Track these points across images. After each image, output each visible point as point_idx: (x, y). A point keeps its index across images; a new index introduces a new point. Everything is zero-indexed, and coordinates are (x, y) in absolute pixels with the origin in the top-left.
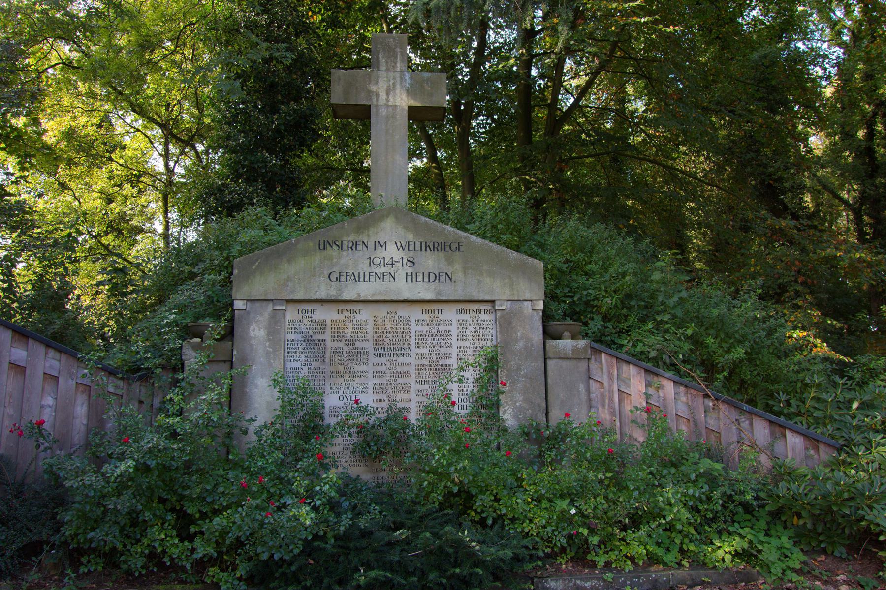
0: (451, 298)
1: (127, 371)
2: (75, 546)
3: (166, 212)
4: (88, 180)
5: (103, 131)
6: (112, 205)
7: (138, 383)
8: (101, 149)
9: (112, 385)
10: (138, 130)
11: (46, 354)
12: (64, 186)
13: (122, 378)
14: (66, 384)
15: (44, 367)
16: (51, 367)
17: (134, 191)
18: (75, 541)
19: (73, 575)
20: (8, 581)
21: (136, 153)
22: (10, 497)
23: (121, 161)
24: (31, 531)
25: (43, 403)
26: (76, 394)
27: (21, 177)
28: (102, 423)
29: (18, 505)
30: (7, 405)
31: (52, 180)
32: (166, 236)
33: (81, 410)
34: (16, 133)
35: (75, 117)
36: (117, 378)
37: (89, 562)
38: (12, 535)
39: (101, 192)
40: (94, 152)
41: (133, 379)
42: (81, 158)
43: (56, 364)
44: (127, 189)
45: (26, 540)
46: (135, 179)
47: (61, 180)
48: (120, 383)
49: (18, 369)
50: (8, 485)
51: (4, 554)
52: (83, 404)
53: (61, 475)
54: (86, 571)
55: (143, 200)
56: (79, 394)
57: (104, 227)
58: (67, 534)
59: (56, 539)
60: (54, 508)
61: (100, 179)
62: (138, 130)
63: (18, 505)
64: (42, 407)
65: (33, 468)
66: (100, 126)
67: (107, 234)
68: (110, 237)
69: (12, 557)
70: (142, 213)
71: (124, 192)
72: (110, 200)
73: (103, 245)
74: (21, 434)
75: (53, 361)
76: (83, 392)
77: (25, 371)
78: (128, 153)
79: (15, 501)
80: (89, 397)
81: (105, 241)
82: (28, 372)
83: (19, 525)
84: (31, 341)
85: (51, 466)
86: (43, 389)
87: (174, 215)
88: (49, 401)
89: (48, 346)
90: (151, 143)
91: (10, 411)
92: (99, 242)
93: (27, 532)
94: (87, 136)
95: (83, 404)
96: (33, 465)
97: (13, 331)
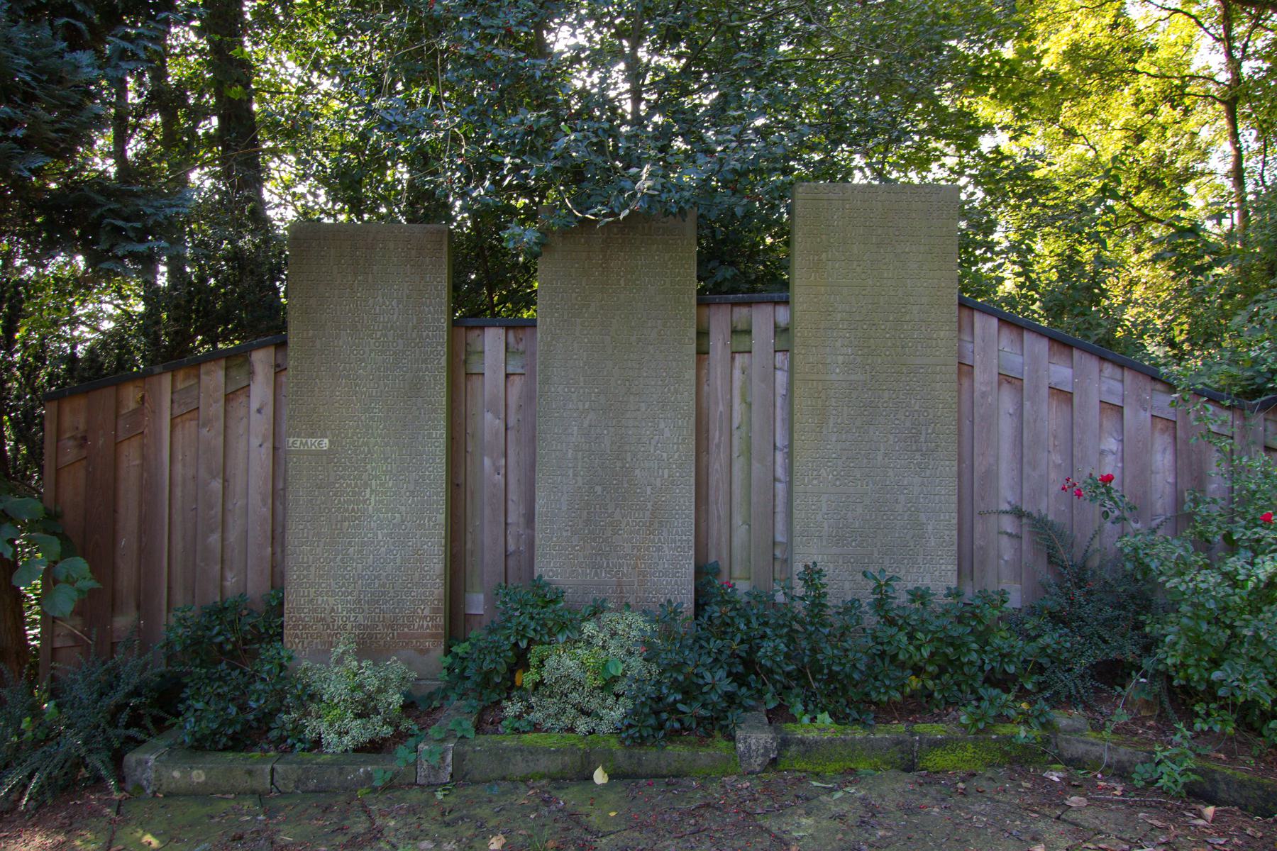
0: (174, 511)
1: (1237, 395)
2: (1183, 682)
3: (1235, 135)
4: (1103, 115)
5: (1120, 32)
6: (1143, 145)
7: (1262, 415)
8: (1121, 60)
9: (1217, 419)
10: (1176, 11)
11: (1101, 371)
12: (1070, 133)
13: (1228, 408)
14: (1136, 418)
15: (1100, 392)
16: (1110, 392)
17: (1178, 113)
18: (1181, 674)
19: (1188, 734)
20: (1080, 710)
21: (1175, 50)
22: (1069, 584)
23: (1153, 71)
24: (1105, 641)
25: (1102, 447)
26: (1153, 433)
27: (1021, 128)
28: (1200, 481)
29: (1082, 599)
30: (1051, 449)
31: (1055, 128)
32: (1238, 174)
33: (1162, 460)
34: (1007, 68)
35: (1078, 25)
36: (1222, 407)
37: (1208, 714)
38: (1078, 643)
39: (1125, 128)
40: (1111, 68)
41: (1252, 409)
42: (1093, 83)
43: (1117, 386)
44: (1166, 113)
45: (1100, 656)
46: (1175, 96)
47: (1067, 126)
48: (1226, 416)
49: (1062, 395)
50: (1065, 568)
51: (1070, 670)
52: (1165, 449)
53: (1153, 566)
54: (1206, 728)
55: (1191, 125)
56: (1157, 434)
57: (1134, 182)
58: (1169, 661)
59: (1147, 663)
60: (1138, 613)
61: (1122, 109)
62: (1176, 11)
63: (1082, 599)
64: (1102, 453)
65: (1096, 545)
66: (1114, 26)
67: (1139, 190)
68: (1144, 195)
69: (1082, 677)
70: (1190, 147)
71: (1161, 120)
72: (1139, 137)
73: (1135, 209)
74: (1079, 494)
75: (1112, 382)
76: (1163, 431)
77: (1071, 400)
78: (1162, 54)
79: (1077, 593)
80: (1175, 438)
81: (1137, 202)
82: (1076, 400)
83: (1087, 630)
84: (1076, 353)
85: (1136, 549)
86: (1101, 426)
87: (1249, 138)
88: (1111, 444)
89: (1103, 359)
90: (1200, 24)
91: (1057, 458)
92: (1130, 205)
93: (1100, 642)
94: (1098, 46)
95: (1165, 449)
96: (1097, 540)
97: (1050, 339)
